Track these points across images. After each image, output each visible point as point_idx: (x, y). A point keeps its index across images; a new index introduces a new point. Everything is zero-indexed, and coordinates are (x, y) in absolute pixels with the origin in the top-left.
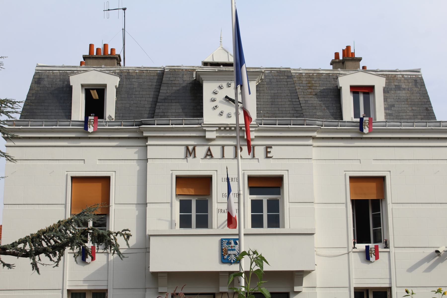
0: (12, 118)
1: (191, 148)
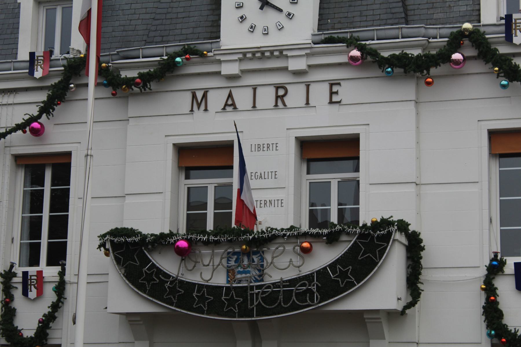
1: (199, 95)
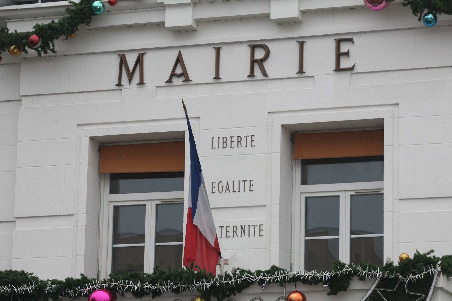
0: (430, 26)
1: (131, 60)
